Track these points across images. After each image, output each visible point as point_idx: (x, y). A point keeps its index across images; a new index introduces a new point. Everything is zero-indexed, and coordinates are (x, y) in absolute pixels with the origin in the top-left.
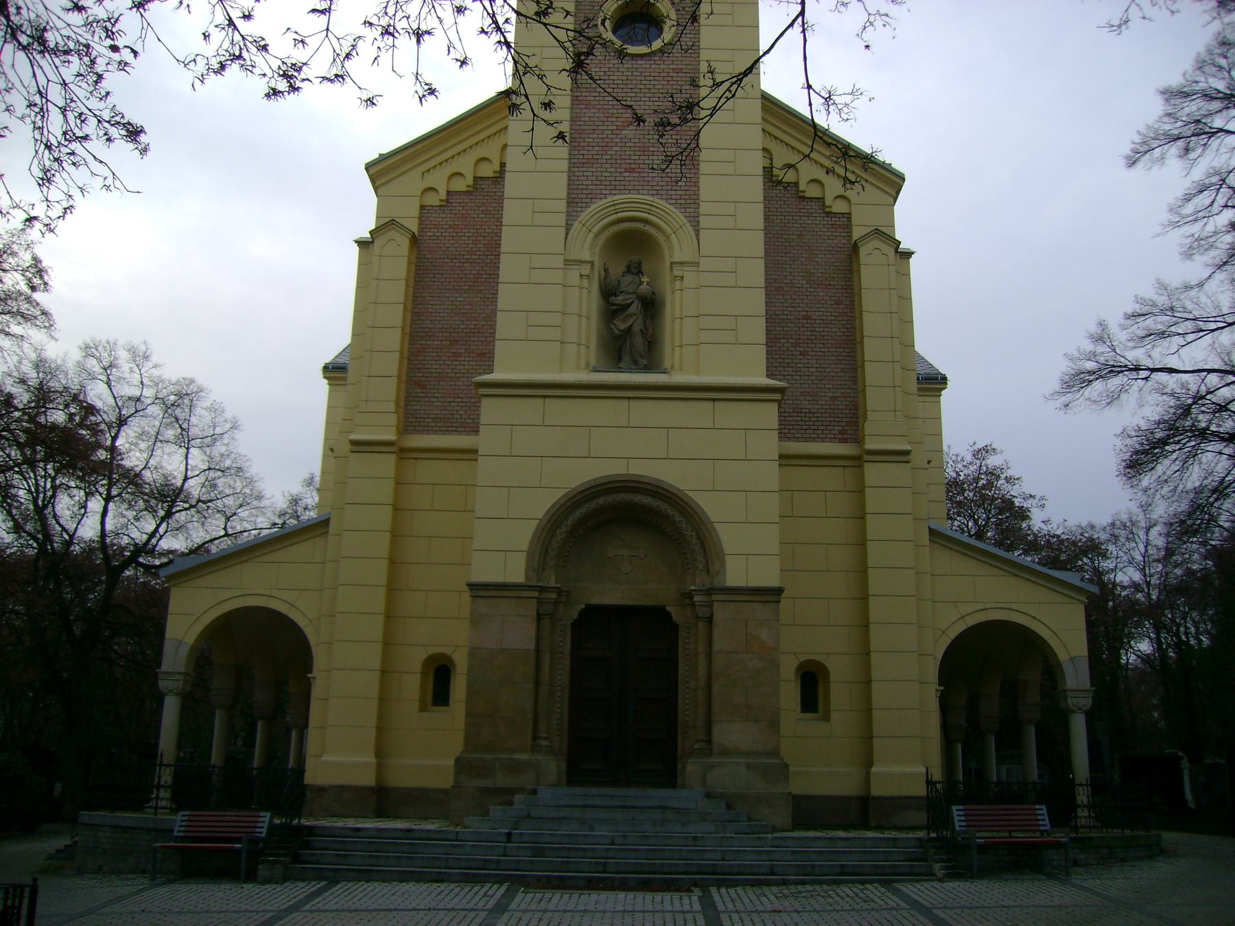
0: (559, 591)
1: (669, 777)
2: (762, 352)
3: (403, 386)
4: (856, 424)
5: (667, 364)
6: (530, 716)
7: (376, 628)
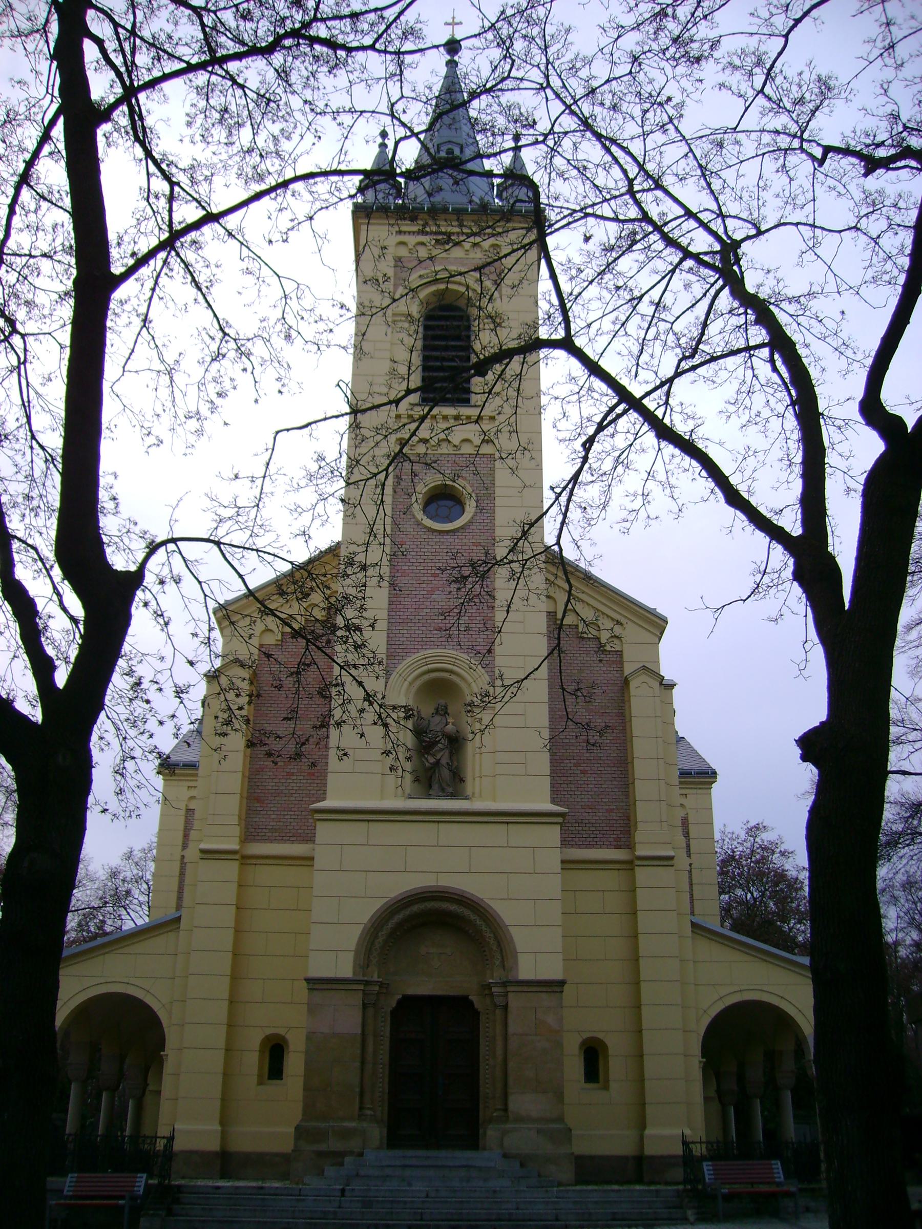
0: (381, 985)
1: (473, 1141)
2: (547, 781)
3: (245, 801)
4: (629, 832)
5: (469, 792)
6: (357, 1090)
7: (221, 1011)
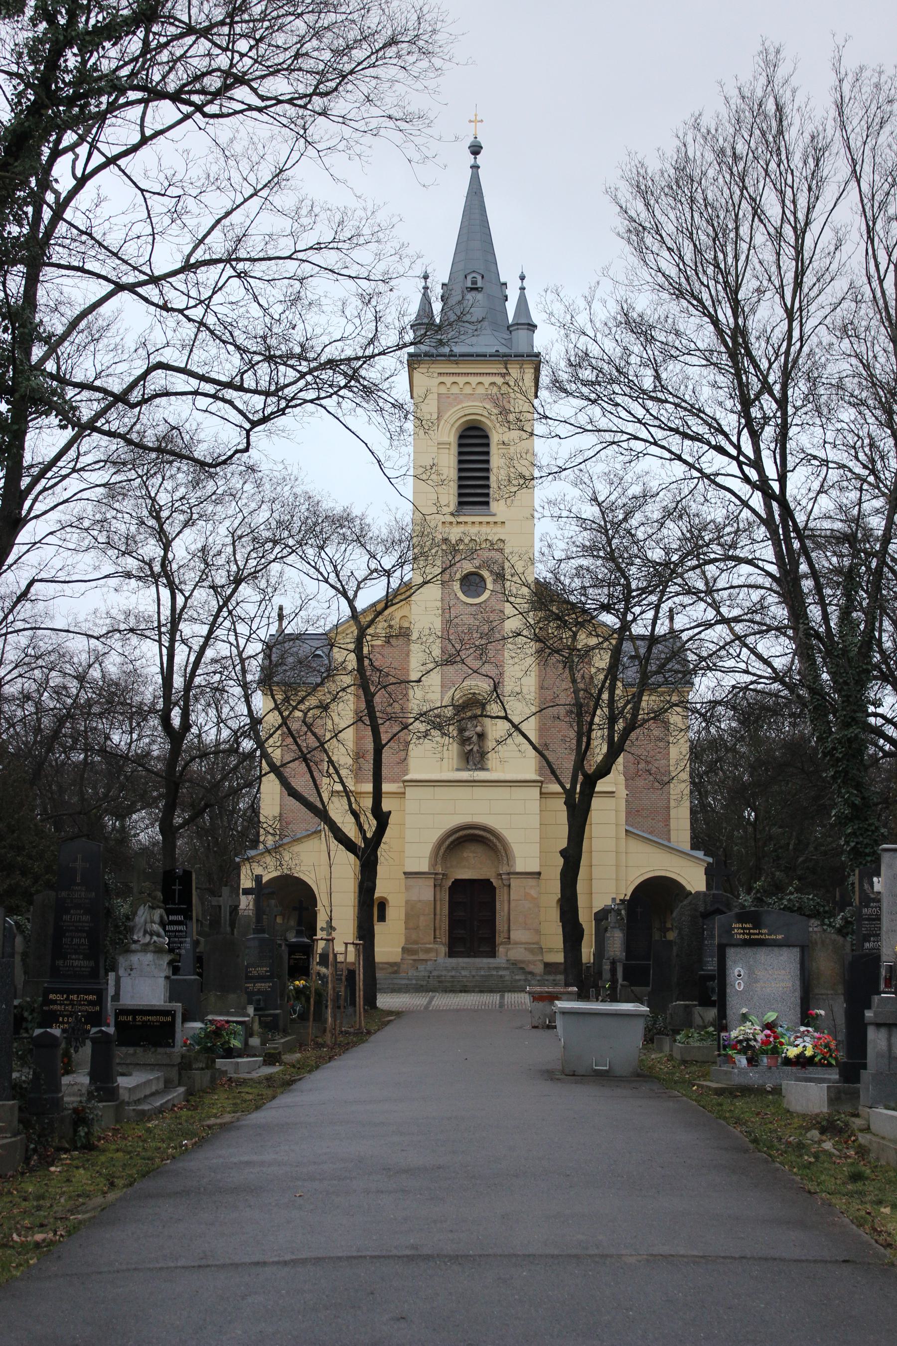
0: (443, 875)
1: (493, 954)
5: (489, 767)
